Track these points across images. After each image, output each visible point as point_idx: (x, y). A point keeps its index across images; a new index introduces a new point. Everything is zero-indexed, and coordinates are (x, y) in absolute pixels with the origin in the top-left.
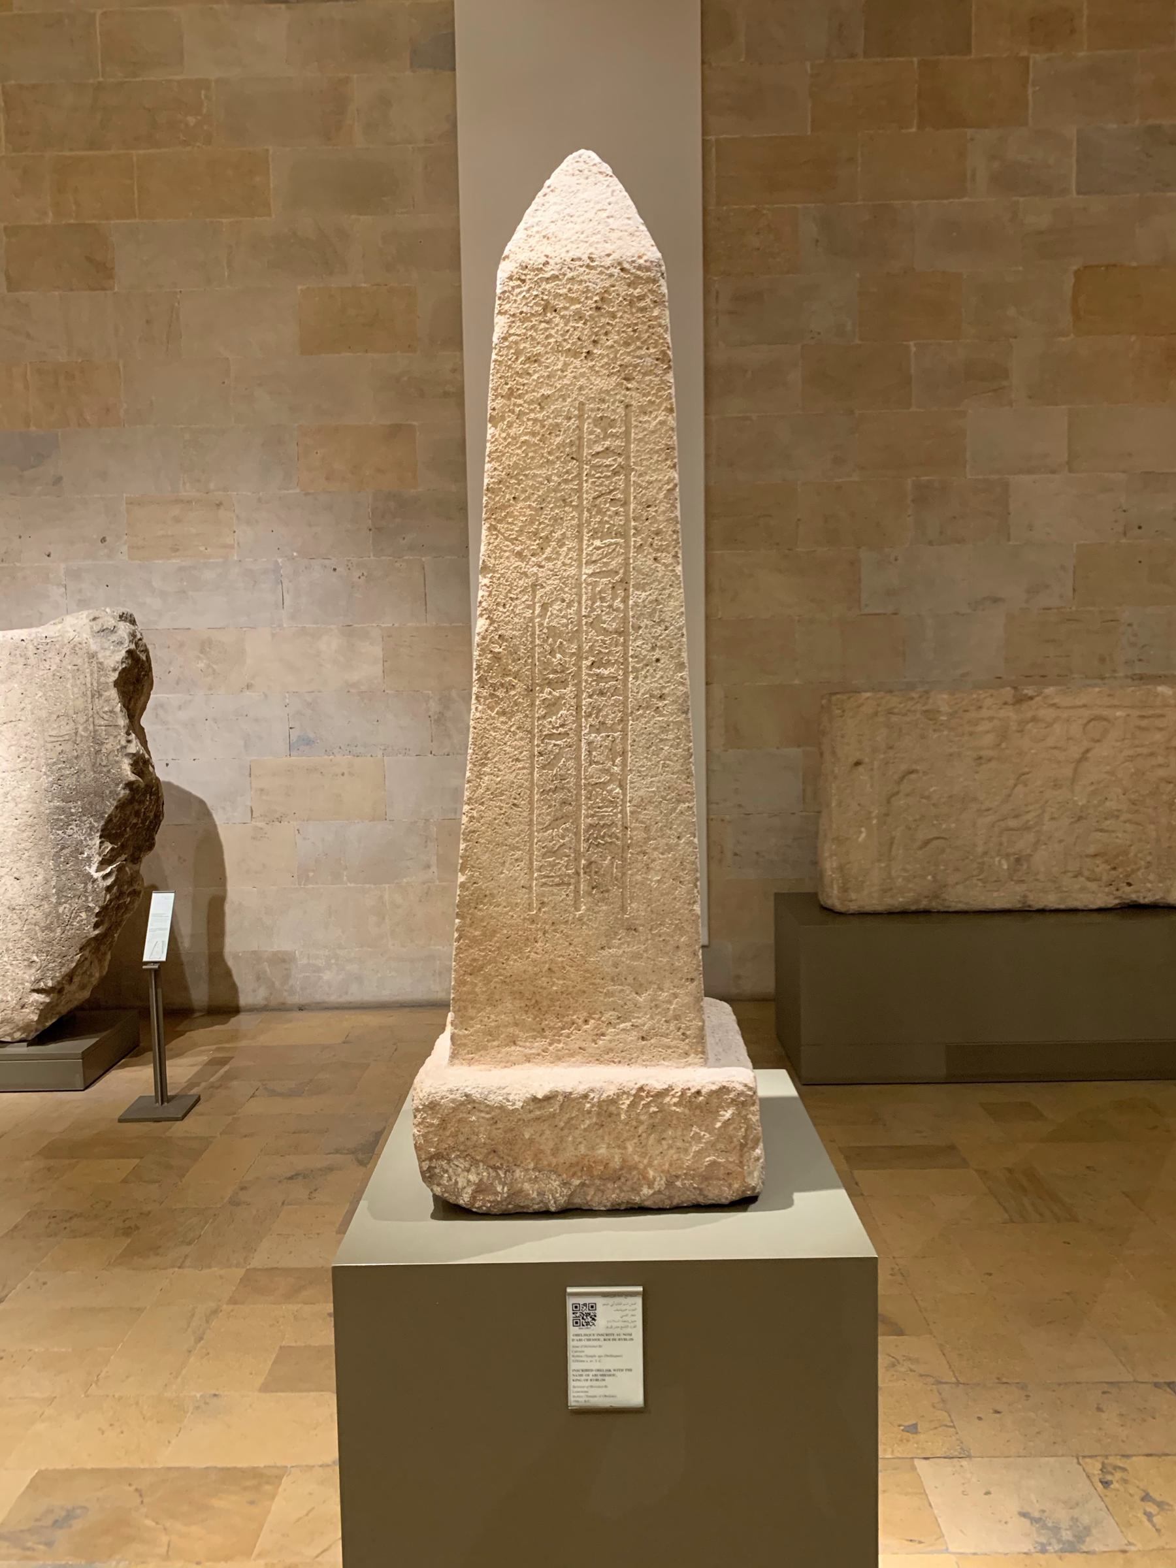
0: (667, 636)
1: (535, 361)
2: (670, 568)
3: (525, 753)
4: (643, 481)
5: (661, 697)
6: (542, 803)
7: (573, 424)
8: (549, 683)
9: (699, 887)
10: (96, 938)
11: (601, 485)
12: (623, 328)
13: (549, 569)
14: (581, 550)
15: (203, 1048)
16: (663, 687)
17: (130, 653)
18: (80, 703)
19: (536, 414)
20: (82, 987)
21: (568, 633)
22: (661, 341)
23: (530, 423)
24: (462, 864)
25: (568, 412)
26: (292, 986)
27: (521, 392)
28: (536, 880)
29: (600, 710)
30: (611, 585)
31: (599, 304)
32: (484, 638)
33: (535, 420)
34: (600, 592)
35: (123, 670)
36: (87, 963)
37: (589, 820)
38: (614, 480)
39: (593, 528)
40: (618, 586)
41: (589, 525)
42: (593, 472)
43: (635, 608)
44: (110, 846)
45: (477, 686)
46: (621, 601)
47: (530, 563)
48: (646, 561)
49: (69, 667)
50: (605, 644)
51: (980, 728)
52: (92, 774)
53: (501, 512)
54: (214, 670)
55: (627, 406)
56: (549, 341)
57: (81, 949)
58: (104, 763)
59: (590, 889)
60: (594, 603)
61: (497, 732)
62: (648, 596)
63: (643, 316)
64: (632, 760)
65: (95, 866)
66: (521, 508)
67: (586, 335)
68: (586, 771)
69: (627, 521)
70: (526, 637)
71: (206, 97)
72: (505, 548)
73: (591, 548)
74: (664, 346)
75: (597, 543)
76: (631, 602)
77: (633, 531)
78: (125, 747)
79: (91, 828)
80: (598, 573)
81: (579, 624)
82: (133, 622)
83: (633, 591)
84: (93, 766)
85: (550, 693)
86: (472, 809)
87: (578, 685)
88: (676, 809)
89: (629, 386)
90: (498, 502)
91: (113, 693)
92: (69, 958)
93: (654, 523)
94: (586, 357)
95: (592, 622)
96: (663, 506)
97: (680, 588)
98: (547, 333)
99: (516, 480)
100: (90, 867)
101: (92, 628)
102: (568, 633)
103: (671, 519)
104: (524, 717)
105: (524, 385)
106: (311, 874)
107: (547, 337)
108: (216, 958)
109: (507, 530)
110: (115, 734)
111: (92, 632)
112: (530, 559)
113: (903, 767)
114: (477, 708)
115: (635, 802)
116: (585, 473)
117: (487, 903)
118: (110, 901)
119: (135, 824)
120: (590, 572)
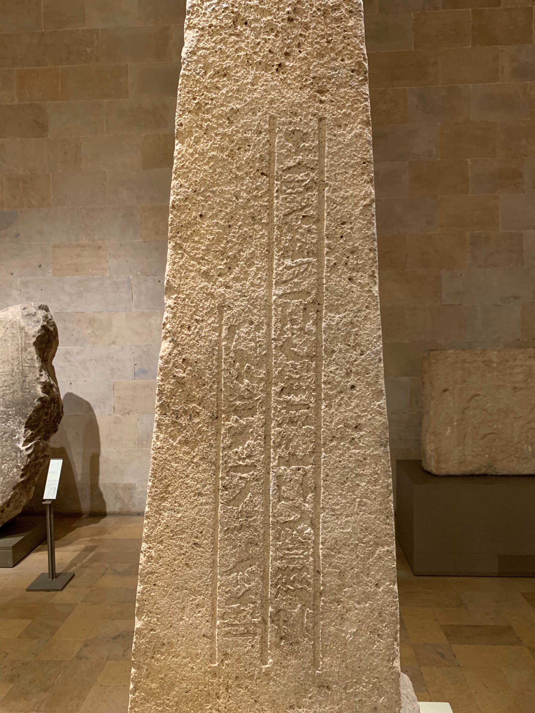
0: (363, 361)
1: (225, 75)
2: (366, 289)
3: (208, 487)
4: (336, 197)
5: (357, 428)
6: (226, 542)
7: (264, 138)
8: (235, 410)
9: (399, 640)
10: (22, 482)
11: (292, 201)
12: (316, 39)
13: (236, 290)
14: (271, 270)
15: (82, 539)
16: (359, 416)
17: (43, 327)
18: (15, 355)
19: (224, 128)
20: (16, 508)
21: (257, 357)
22: (357, 52)
23: (218, 138)
24: (138, 608)
25: (258, 127)
26: (134, 502)
27: (208, 106)
28: (219, 628)
29: (291, 440)
30: (302, 307)
31: (292, 15)
32: (167, 362)
33: (224, 135)
34: (291, 314)
35: (39, 336)
36: (18, 496)
37: (278, 564)
38: (306, 195)
39: (284, 247)
40: (310, 308)
41: (279, 243)
42: (284, 188)
43: (328, 331)
44: (30, 432)
45: (159, 413)
46: (313, 324)
47: (217, 283)
48: (340, 281)
49: (10, 335)
50: (296, 369)
51: (516, 371)
52: (21, 393)
53: (187, 230)
54: (96, 334)
55: (321, 120)
56: (240, 54)
57: (14, 489)
58: (27, 387)
59: (278, 639)
60: (284, 325)
61: (178, 463)
62: (342, 319)
63: (338, 27)
64: (325, 497)
65: (22, 443)
66: (207, 226)
67: (278, 47)
68: (274, 507)
69: (320, 239)
70: (212, 362)
71: (96, 38)
72: (191, 268)
73: (281, 268)
74: (361, 57)
75: (288, 262)
76: (324, 324)
77: (326, 250)
78: (39, 378)
79: (20, 422)
80: (289, 293)
81: (269, 348)
82: (47, 310)
83: (326, 314)
84: (21, 388)
85: (237, 421)
86: (150, 548)
87: (266, 412)
88: (373, 553)
89: (323, 98)
90: (184, 219)
91: (33, 349)
92: (7, 493)
93: (349, 241)
94: (277, 70)
95: (282, 346)
96: (360, 223)
97: (377, 309)
98: (237, 47)
99: (203, 196)
100: (19, 444)
101: (22, 313)
102: (257, 357)
103: (368, 237)
104: (208, 447)
105: (212, 99)
106: (145, 442)
107: (237, 51)
108: (95, 486)
109: (193, 248)
110: (34, 371)
111: (22, 316)
112: (217, 279)
113: (472, 393)
114: (157, 437)
115: (327, 545)
116: (276, 189)
117: (165, 652)
118: (30, 462)
119: (45, 420)
120: (281, 292)
